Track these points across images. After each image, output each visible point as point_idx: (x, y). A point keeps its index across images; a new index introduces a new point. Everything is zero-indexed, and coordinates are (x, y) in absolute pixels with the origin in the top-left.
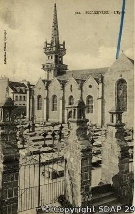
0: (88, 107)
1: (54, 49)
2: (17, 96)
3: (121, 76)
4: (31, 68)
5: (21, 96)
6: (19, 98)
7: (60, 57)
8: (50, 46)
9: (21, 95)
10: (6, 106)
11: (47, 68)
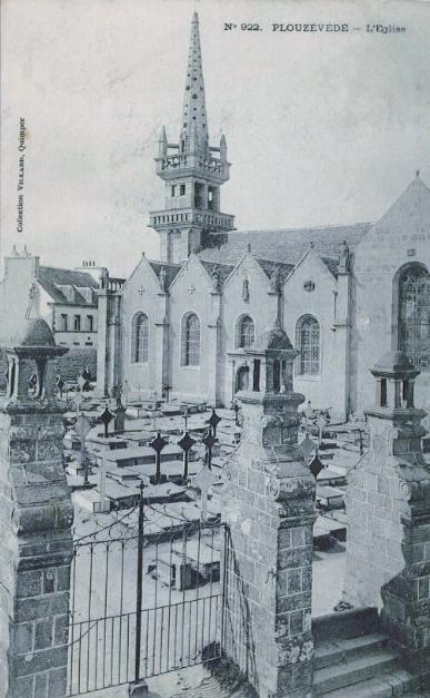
2: (64, 316)
7: (211, 189)
8: (176, 152)
9: (78, 311)
11: (166, 224)
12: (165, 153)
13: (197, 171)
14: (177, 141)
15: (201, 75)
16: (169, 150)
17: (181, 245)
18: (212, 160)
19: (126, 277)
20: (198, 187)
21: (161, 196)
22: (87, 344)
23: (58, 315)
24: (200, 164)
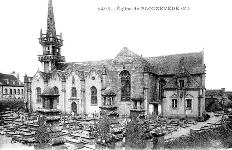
0: (144, 89)
1: (51, 40)
2: (6, 89)
3: (124, 68)
4: (25, 62)
5: (15, 90)
6: (9, 92)
7: (57, 48)
8: (45, 36)
9: (11, 88)
10: (163, 137)
11: (44, 60)
12: (42, 37)
13: (51, 42)
14: (45, 33)
15: (53, 12)
16: (43, 35)
17: (50, 66)
18: (58, 39)
19: (33, 77)
20: (53, 48)
21: (40, 50)
22: (14, 98)
23: (4, 89)
24: (54, 41)
